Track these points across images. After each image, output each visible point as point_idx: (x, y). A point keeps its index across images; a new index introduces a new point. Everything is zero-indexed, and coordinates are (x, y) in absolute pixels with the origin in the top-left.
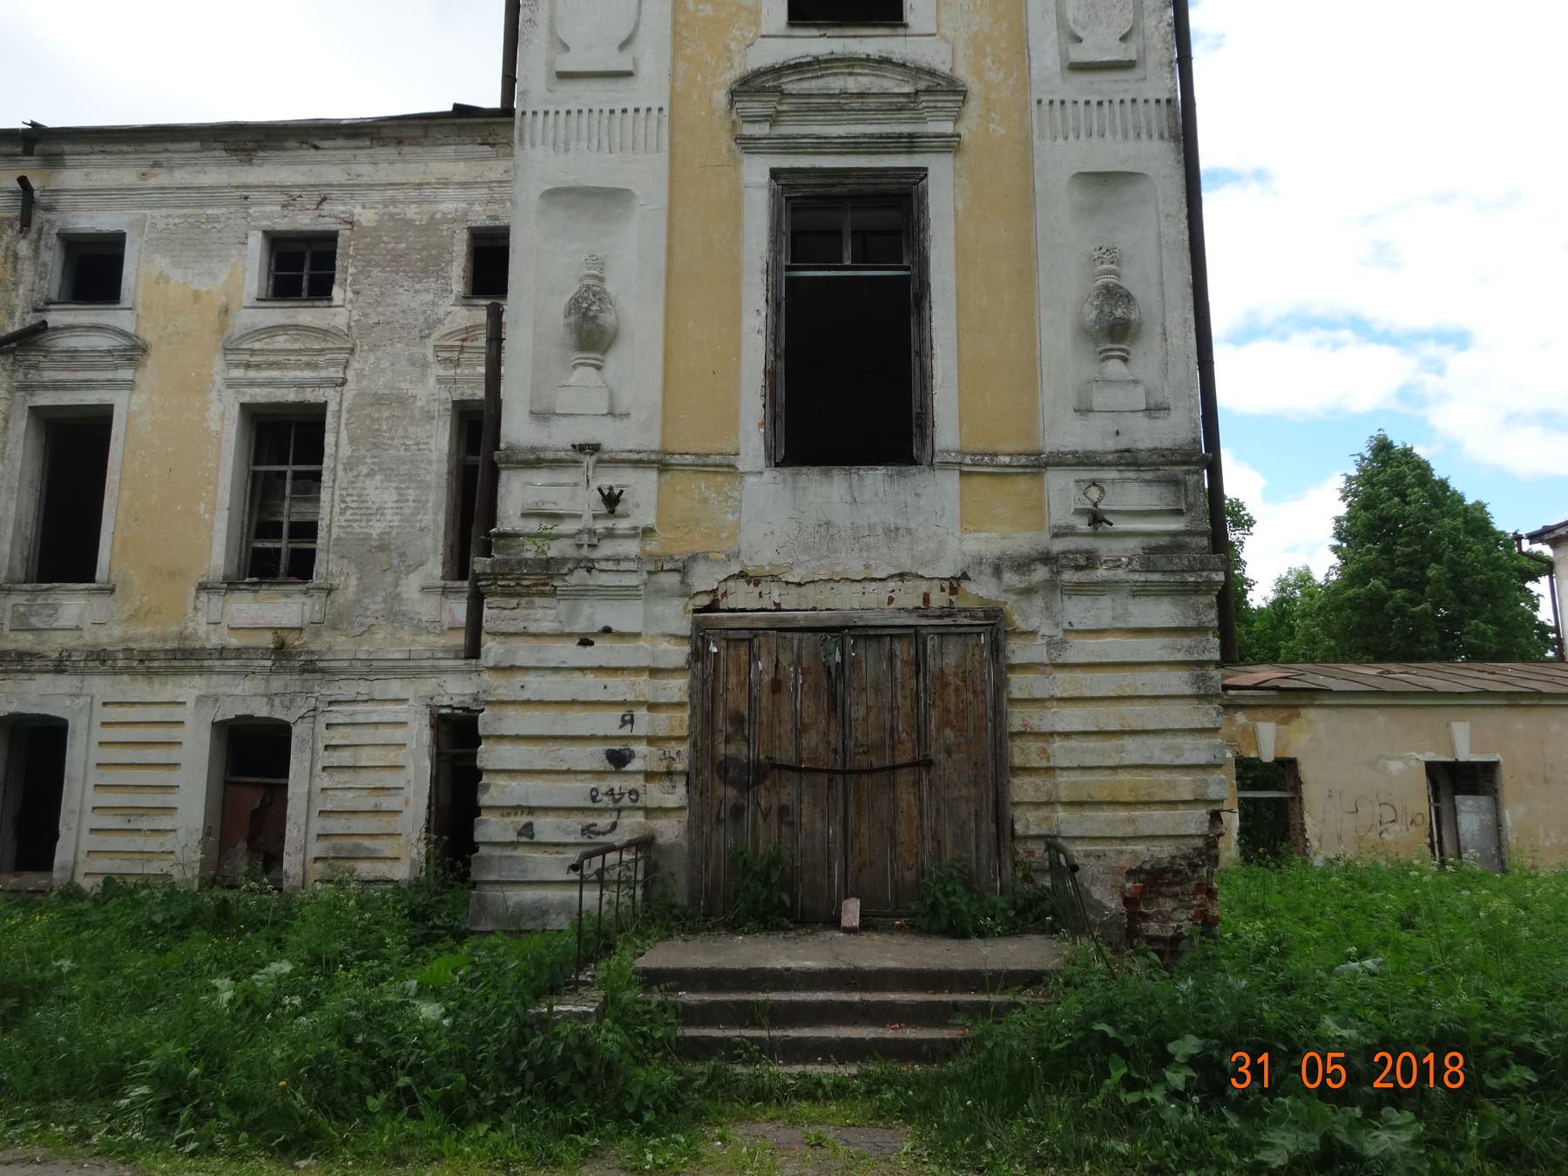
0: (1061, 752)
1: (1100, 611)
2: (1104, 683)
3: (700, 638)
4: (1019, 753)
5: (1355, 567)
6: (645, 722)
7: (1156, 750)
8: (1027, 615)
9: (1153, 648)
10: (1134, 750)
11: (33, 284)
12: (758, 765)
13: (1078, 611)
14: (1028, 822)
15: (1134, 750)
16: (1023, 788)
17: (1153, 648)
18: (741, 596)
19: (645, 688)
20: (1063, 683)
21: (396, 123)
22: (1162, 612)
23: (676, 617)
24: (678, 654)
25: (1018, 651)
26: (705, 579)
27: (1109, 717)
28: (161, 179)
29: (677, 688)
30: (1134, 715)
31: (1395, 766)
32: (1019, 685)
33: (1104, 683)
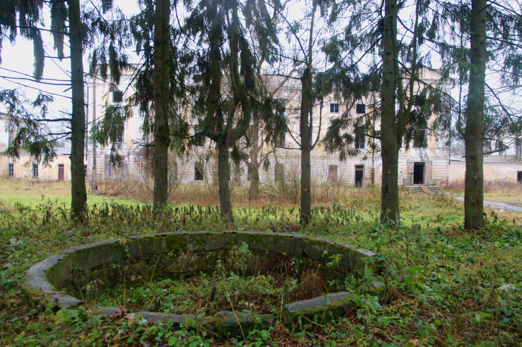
0: (436, 172)
1: (440, 161)
2: (440, 167)
3: (408, 163)
4: (433, 172)
5: (252, 51)
6: (404, 169)
7: (443, 172)
8: (434, 161)
9: (444, 164)
10: (442, 172)
11: (135, 159)
12: (381, 23)
13: (438, 161)
14: (433, 178)
15: (442, 172)
16: (433, 175)
17: (444, 164)
18: (411, 159)
19: (403, 167)
20: (437, 167)
21: (232, 45)
22: (445, 161)
23: (406, 161)
24: (406, 164)
25: (433, 164)
26: (408, 158)
27: (440, 170)
28: (91, 102)
29: (406, 167)
30: (442, 170)
31: (461, 172)
32: (433, 167)
33: (440, 167)
